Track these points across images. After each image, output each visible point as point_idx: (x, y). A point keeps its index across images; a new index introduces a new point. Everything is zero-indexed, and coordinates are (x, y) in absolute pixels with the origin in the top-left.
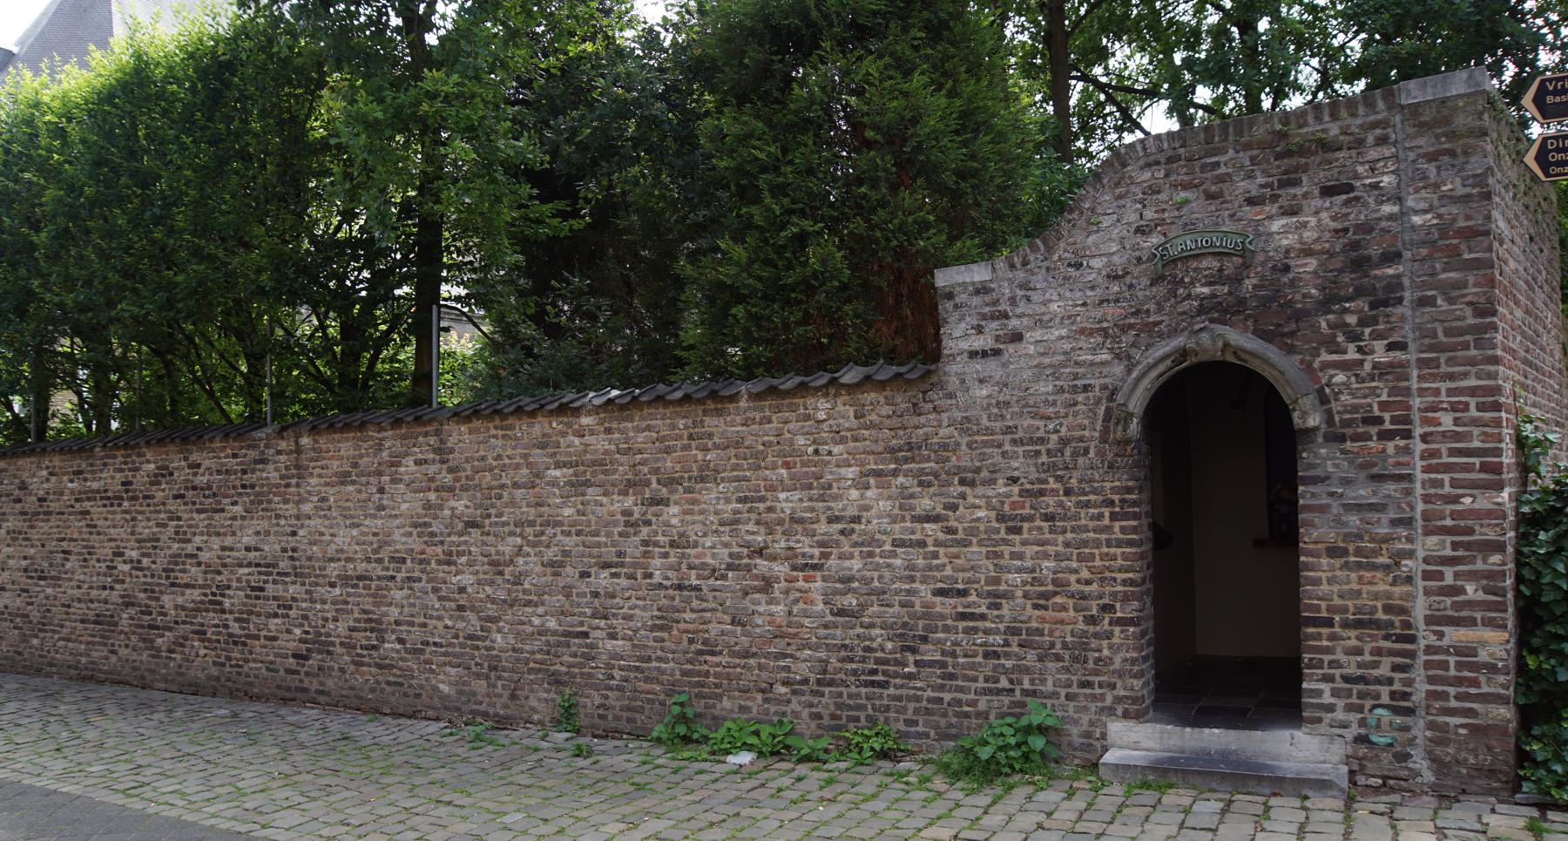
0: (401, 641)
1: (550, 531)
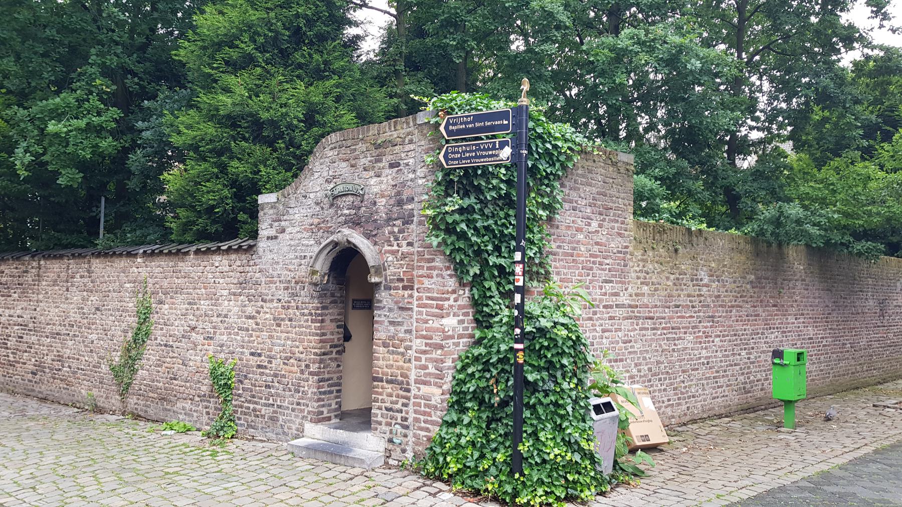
0: (70, 367)
1: (124, 314)
